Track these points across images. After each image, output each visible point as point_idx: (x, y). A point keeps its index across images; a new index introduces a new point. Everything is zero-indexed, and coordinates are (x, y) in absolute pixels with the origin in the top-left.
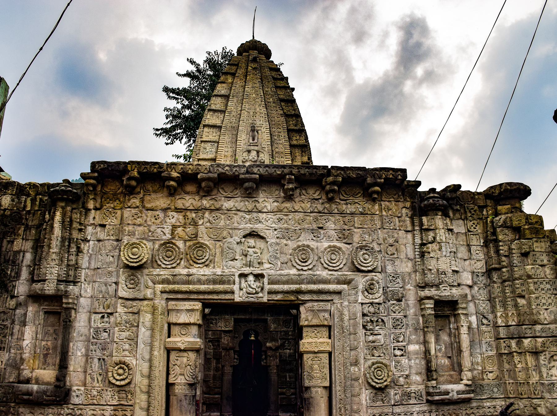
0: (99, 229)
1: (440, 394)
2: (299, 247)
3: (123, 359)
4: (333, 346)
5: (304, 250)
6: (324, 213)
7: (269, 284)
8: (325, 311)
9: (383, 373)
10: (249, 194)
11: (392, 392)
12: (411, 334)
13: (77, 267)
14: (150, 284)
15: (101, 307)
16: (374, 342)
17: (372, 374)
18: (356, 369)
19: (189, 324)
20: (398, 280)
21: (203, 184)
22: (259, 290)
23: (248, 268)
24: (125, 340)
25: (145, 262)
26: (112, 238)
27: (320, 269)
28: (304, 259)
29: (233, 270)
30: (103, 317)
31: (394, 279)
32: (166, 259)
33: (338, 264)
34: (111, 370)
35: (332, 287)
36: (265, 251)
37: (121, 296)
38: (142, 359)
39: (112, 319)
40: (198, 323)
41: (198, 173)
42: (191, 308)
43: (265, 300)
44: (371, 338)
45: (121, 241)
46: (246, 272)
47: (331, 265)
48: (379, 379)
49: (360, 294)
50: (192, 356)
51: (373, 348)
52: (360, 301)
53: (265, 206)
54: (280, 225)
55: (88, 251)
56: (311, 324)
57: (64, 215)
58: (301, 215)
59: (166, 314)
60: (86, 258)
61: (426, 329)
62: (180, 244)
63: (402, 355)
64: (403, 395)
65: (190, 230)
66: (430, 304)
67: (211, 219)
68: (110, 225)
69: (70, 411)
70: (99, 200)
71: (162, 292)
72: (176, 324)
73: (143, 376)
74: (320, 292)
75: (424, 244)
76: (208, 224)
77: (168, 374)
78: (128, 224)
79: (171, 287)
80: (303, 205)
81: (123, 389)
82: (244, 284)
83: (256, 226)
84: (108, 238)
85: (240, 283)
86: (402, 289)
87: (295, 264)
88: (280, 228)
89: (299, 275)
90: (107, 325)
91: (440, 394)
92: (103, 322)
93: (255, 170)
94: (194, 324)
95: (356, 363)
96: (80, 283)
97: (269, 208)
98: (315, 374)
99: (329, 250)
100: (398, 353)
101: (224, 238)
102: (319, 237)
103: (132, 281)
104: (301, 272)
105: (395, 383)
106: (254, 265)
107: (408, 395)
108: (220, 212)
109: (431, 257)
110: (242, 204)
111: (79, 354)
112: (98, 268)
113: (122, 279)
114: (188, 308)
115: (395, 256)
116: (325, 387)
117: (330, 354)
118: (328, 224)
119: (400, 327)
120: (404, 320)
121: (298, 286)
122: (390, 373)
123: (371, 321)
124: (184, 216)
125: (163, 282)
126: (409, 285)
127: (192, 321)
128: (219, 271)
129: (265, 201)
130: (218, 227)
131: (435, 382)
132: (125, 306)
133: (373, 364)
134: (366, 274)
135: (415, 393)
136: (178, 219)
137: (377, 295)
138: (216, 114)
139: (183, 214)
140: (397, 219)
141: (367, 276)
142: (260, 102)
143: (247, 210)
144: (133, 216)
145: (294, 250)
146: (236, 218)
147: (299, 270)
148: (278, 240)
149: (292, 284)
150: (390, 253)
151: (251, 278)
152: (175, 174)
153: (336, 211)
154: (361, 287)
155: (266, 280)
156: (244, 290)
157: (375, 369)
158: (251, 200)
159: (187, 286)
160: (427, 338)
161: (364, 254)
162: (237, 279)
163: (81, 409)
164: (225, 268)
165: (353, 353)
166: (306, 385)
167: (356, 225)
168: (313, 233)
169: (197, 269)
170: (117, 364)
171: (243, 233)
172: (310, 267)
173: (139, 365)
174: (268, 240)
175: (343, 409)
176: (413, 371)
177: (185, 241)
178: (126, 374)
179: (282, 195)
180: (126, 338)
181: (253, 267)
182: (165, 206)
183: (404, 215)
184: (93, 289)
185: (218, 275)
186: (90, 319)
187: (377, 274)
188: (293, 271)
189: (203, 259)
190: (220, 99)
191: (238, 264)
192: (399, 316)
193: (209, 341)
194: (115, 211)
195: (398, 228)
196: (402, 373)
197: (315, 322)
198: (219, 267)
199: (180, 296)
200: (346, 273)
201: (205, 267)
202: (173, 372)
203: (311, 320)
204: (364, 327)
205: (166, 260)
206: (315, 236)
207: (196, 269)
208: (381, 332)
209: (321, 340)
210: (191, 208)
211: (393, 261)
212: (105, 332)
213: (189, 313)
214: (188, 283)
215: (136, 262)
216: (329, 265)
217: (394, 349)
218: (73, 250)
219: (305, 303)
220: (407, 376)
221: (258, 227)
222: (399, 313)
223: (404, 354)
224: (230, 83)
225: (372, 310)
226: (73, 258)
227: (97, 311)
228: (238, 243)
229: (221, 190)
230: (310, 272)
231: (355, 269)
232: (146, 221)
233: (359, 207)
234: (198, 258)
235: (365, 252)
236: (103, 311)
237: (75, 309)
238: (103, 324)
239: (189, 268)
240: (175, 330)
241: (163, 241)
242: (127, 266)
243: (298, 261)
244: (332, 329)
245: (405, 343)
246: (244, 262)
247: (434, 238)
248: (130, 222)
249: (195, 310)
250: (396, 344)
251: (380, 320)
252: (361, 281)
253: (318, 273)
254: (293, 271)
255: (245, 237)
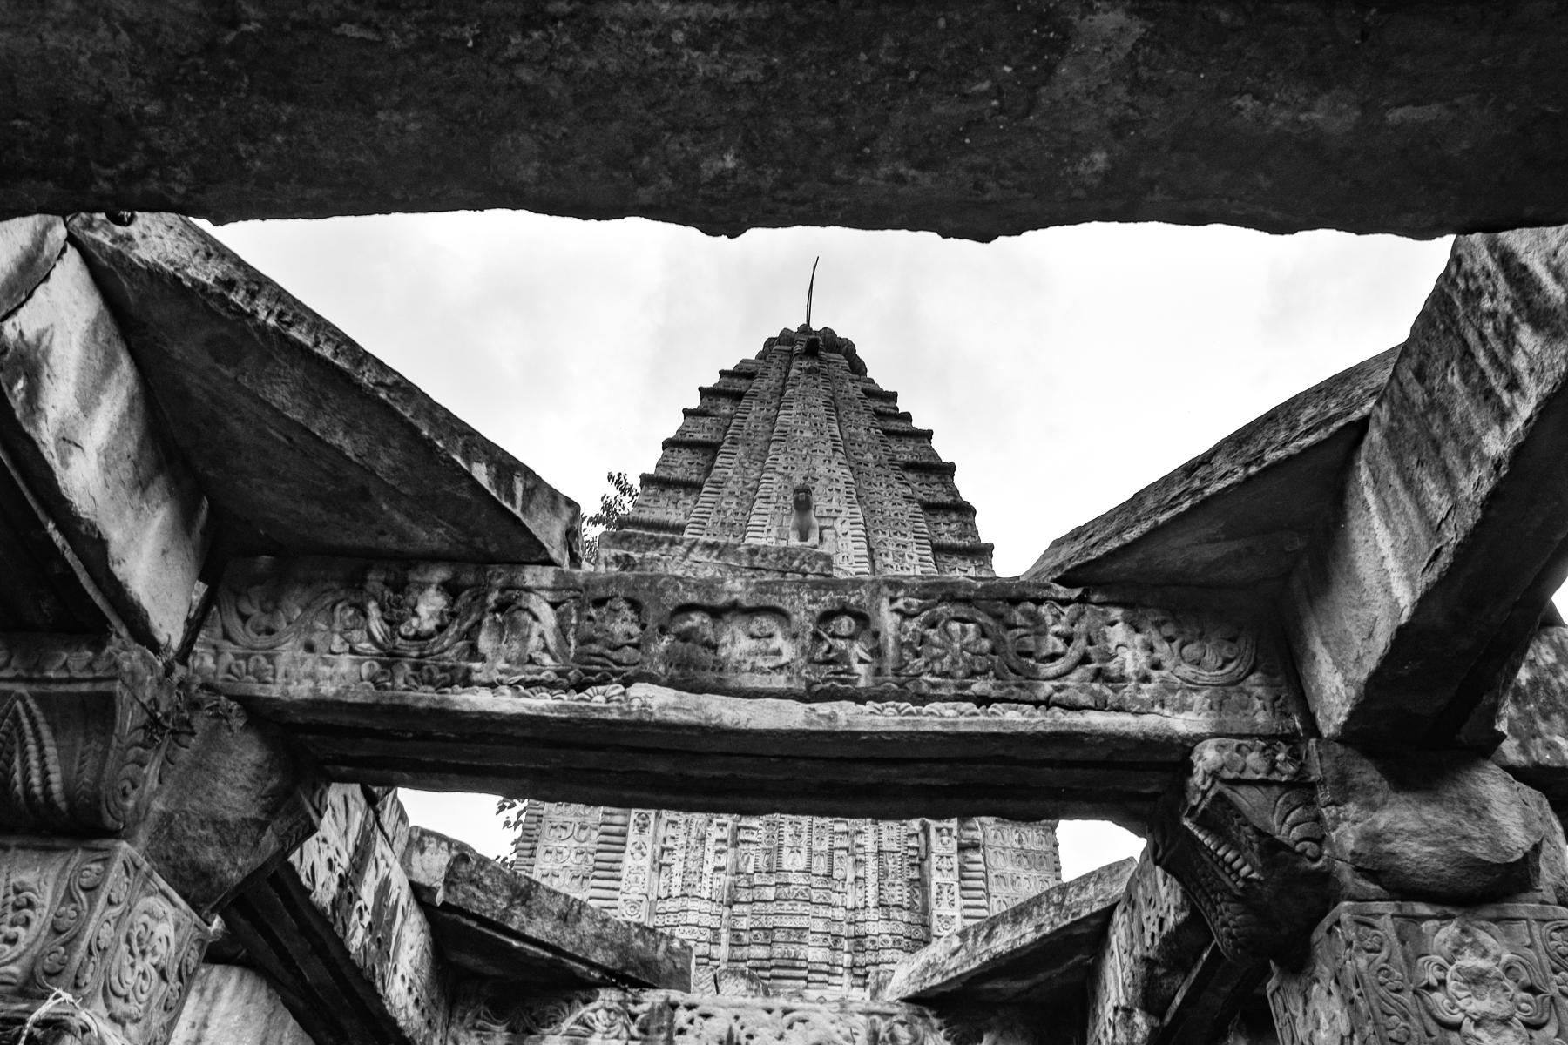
138: (670, 493)
142: (829, 452)
190: (686, 453)
224: (725, 416)
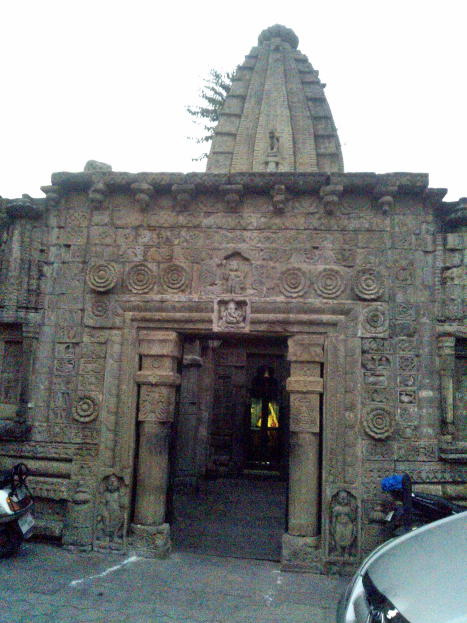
0: (63, 250)
1: (456, 451)
2: (289, 270)
3: (87, 394)
4: (324, 387)
5: (294, 274)
6: (320, 230)
7: (252, 312)
8: (318, 345)
9: (385, 422)
10: (234, 209)
11: (396, 446)
12: (423, 378)
13: (38, 293)
14: (120, 311)
15: (66, 337)
16: (375, 384)
17: (370, 421)
18: (352, 415)
19: (162, 356)
20: (411, 312)
21: (179, 197)
22: (241, 319)
23: (229, 294)
24: (91, 373)
25: (113, 288)
26: (78, 259)
27: (312, 296)
28: (293, 285)
29: (211, 296)
30: (68, 347)
31: (404, 310)
32: (138, 283)
33: (334, 291)
34: (75, 406)
35: (325, 318)
36: (249, 275)
37: (86, 324)
38: (109, 395)
39: (78, 350)
40: (172, 355)
41: (172, 184)
44: (372, 379)
45: (87, 263)
46: (226, 299)
47: (326, 291)
48: (379, 429)
49: (360, 326)
50: (164, 391)
51: (373, 391)
52: (359, 334)
53: (251, 223)
54: (267, 245)
55: (52, 274)
57: (22, 234)
58: (293, 233)
59: (137, 345)
60: (50, 283)
61: (442, 372)
62: (153, 266)
63: (411, 402)
64: (408, 450)
65: (164, 251)
66: (450, 342)
67: (188, 238)
68: (75, 245)
69: (32, 448)
70: (63, 218)
71: (132, 320)
72: (147, 356)
73: (109, 412)
74: (311, 323)
75: (448, 268)
76: (185, 244)
77: (138, 410)
78: (95, 244)
79: (143, 314)
80: (296, 221)
81: (89, 426)
82: (224, 314)
83: (240, 246)
84: (72, 260)
85: (219, 311)
86: (415, 323)
87: (283, 290)
88: (267, 248)
89: (288, 303)
90: (72, 356)
91: (456, 451)
92: (68, 353)
93: (238, 179)
94: (167, 356)
95: (351, 408)
96: (42, 311)
97: (255, 224)
99: (324, 273)
100: (405, 399)
101: (203, 260)
102: (312, 259)
103: (100, 309)
104: (290, 300)
105: (398, 434)
106: (236, 291)
107: (416, 450)
108: (199, 229)
109: (455, 285)
110: (224, 220)
111: (42, 387)
112: (63, 294)
113: (88, 306)
114: (161, 338)
115: (408, 282)
116: (314, 434)
117: (321, 395)
118: (325, 243)
119: (410, 368)
120: (416, 359)
122: (393, 423)
123: (372, 357)
124: (158, 235)
125: (137, 308)
126: (425, 318)
127: (165, 352)
128: (195, 297)
129: (250, 216)
130: (196, 247)
131: (450, 437)
132: (92, 336)
133: (373, 410)
134: (369, 303)
135: (424, 448)
136: (151, 238)
137: (380, 329)
139: (157, 232)
140: (414, 237)
141: (368, 306)
143: (229, 228)
144: (100, 235)
145: (283, 273)
146: (217, 237)
147: (287, 297)
148: (264, 263)
150: (401, 278)
151: (232, 306)
152: (145, 186)
153: (335, 228)
154: (361, 318)
155: (248, 309)
156: (224, 318)
157: (375, 416)
158: (234, 215)
159: (160, 313)
161: (366, 279)
162: (216, 306)
163: (44, 447)
164: (203, 293)
165: (348, 396)
167: (360, 244)
168: (306, 254)
169: (172, 295)
170: (81, 399)
171: (224, 254)
172: (300, 294)
173: (105, 399)
174: (253, 262)
175: (334, 460)
176: (425, 422)
177: (159, 263)
178: (92, 410)
179: (271, 208)
180: (91, 371)
181: (235, 293)
182: (138, 223)
183: (424, 232)
184: (57, 316)
185: (194, 302)
186: (53, 350)
187: (383, 304)
188: (281, 298)
189: (178, 283)
191: (216, 289)
192: (409, 354)
194: (81, 229)
195: (414, 248)
196: (409, 424)
197: (305, 357)
198: (196, 293)
199: (151, 325)
200: (344, 301)
201: (180, 293)
204: (364, 366)
205: (137, 285)
206: (308, 258)
207: (170, 295)
208: (385, 373)
209: (311, 379)
210: (167, 225)
211: (404, 289)
212: (69, 363)
213: (164, 343)
214: (161, 310)
215: (103, 287)
216: (329, 294)
217: (401, 394)
218: (34, 272)
219: (294, 335)
220: (416, 428)
221: (242, 247)
222: (410, 351)
223: (414, 401)
225: (374, 346)
226: (34, 282)
227: (61, 340)
228: (218, 266)
229: (199, 204)
230: (301, 300)
231: (355, 298)
232: (115, 241)
233: (364, 221)
234: (173, 282)
235: (368, 276)
236: (68, 341)
237: (37, 339)
238: (68, 355)
239: (162, 294)
240: (146, 362)
241: (135, 264)
242: (94, 291)
243: (286, 287)
244: (325, 367)
245: (415, 388)
246: (225, 287)
247: (462, 261)
248: (97, 242)
250: (402, 388)
251: (384, 359)
252: (362, 312)
253: (310, 300)
254: (281, 298)
255: (227, 258)
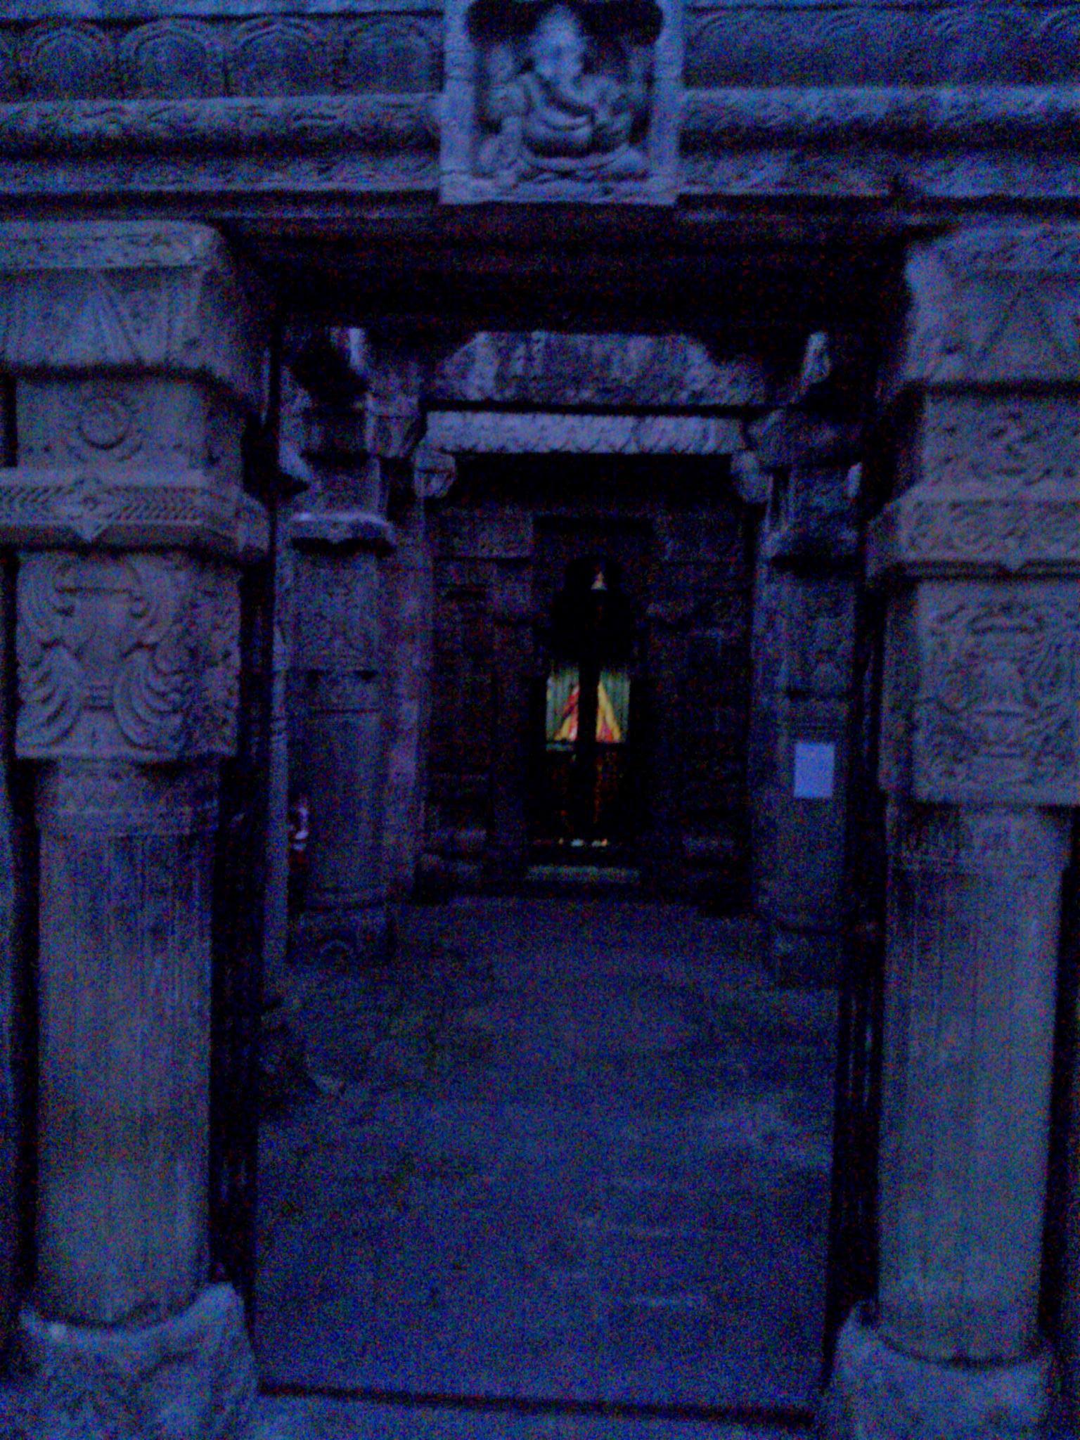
19: (134, 373)
40: (194, 362)
42: (142, 256)
43: (662, 180)
56: (984, 375)
85: (481, 79)
94: (166, 373)
98: (992, 724)
114: (121, 262)
121: (907, 95)
127: (151, 350)
149: (864, 77)
156: (512, 125)
160: (145, 649)
166: (929, 786)
185: (323, 17)
193: (450, 596)
199: (60, 180)
202: (41, 692)
203: (984, 353)
214: (119, 81)
219: (942, 230)
249: (169, 272)
